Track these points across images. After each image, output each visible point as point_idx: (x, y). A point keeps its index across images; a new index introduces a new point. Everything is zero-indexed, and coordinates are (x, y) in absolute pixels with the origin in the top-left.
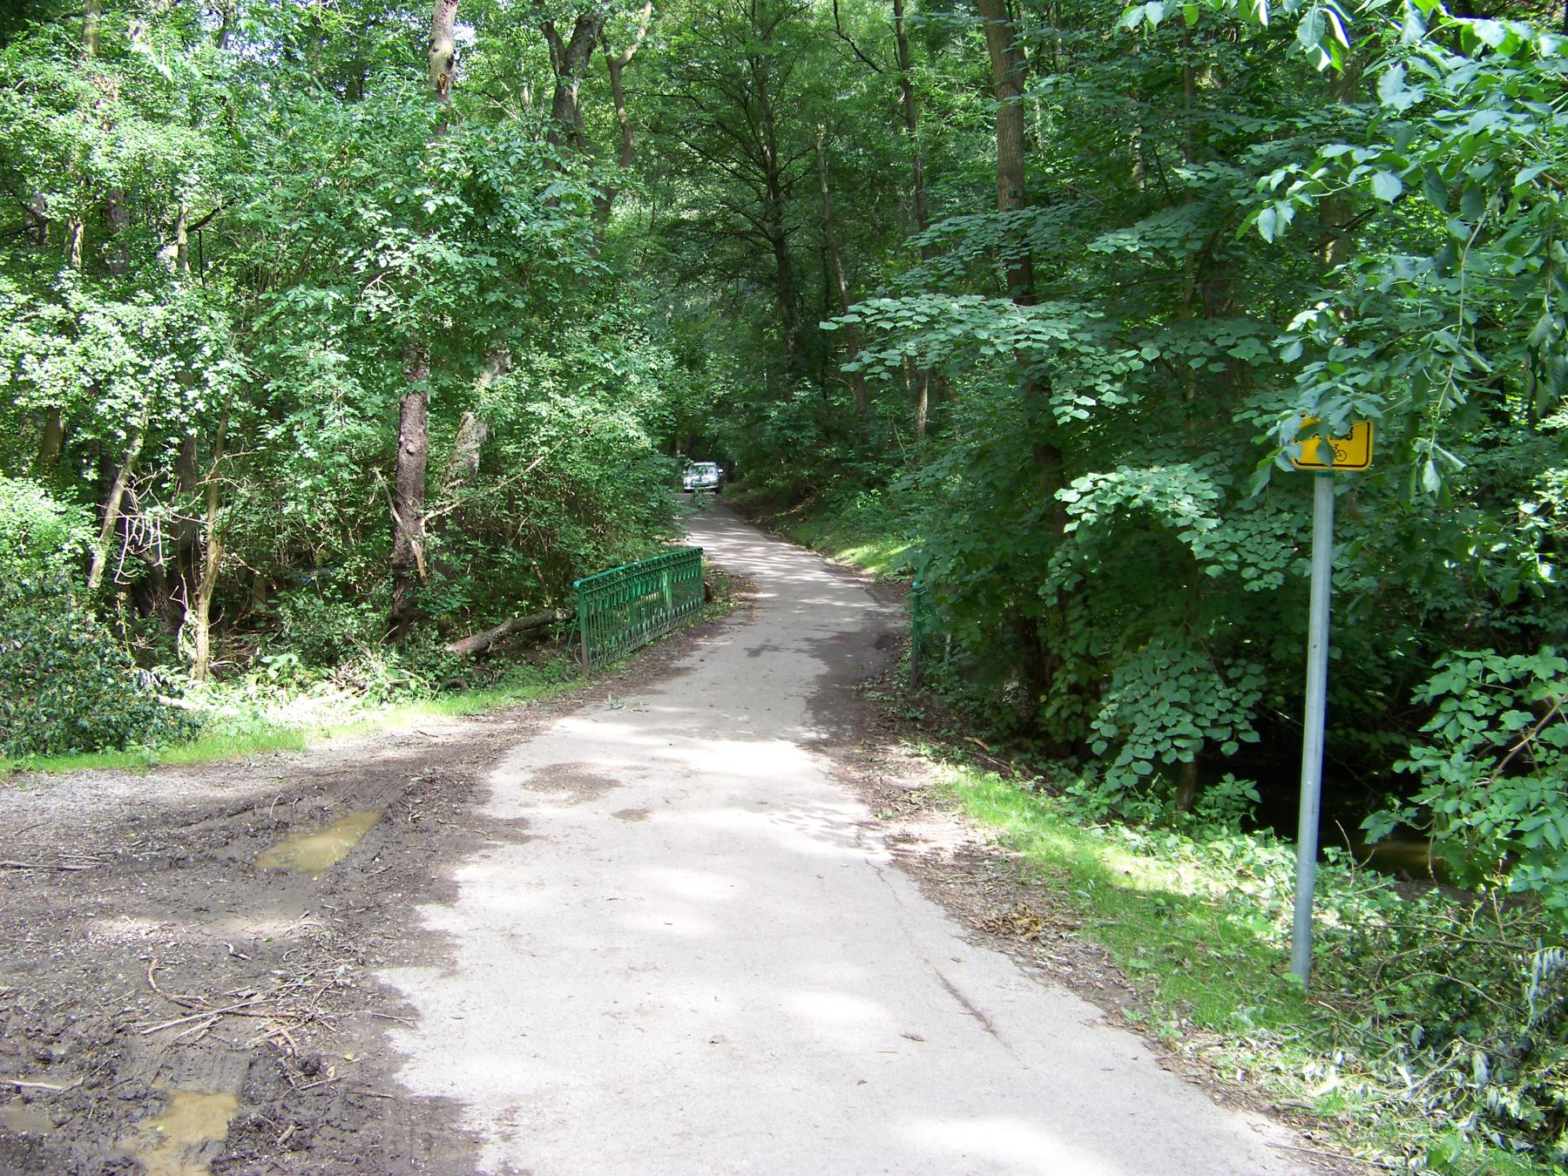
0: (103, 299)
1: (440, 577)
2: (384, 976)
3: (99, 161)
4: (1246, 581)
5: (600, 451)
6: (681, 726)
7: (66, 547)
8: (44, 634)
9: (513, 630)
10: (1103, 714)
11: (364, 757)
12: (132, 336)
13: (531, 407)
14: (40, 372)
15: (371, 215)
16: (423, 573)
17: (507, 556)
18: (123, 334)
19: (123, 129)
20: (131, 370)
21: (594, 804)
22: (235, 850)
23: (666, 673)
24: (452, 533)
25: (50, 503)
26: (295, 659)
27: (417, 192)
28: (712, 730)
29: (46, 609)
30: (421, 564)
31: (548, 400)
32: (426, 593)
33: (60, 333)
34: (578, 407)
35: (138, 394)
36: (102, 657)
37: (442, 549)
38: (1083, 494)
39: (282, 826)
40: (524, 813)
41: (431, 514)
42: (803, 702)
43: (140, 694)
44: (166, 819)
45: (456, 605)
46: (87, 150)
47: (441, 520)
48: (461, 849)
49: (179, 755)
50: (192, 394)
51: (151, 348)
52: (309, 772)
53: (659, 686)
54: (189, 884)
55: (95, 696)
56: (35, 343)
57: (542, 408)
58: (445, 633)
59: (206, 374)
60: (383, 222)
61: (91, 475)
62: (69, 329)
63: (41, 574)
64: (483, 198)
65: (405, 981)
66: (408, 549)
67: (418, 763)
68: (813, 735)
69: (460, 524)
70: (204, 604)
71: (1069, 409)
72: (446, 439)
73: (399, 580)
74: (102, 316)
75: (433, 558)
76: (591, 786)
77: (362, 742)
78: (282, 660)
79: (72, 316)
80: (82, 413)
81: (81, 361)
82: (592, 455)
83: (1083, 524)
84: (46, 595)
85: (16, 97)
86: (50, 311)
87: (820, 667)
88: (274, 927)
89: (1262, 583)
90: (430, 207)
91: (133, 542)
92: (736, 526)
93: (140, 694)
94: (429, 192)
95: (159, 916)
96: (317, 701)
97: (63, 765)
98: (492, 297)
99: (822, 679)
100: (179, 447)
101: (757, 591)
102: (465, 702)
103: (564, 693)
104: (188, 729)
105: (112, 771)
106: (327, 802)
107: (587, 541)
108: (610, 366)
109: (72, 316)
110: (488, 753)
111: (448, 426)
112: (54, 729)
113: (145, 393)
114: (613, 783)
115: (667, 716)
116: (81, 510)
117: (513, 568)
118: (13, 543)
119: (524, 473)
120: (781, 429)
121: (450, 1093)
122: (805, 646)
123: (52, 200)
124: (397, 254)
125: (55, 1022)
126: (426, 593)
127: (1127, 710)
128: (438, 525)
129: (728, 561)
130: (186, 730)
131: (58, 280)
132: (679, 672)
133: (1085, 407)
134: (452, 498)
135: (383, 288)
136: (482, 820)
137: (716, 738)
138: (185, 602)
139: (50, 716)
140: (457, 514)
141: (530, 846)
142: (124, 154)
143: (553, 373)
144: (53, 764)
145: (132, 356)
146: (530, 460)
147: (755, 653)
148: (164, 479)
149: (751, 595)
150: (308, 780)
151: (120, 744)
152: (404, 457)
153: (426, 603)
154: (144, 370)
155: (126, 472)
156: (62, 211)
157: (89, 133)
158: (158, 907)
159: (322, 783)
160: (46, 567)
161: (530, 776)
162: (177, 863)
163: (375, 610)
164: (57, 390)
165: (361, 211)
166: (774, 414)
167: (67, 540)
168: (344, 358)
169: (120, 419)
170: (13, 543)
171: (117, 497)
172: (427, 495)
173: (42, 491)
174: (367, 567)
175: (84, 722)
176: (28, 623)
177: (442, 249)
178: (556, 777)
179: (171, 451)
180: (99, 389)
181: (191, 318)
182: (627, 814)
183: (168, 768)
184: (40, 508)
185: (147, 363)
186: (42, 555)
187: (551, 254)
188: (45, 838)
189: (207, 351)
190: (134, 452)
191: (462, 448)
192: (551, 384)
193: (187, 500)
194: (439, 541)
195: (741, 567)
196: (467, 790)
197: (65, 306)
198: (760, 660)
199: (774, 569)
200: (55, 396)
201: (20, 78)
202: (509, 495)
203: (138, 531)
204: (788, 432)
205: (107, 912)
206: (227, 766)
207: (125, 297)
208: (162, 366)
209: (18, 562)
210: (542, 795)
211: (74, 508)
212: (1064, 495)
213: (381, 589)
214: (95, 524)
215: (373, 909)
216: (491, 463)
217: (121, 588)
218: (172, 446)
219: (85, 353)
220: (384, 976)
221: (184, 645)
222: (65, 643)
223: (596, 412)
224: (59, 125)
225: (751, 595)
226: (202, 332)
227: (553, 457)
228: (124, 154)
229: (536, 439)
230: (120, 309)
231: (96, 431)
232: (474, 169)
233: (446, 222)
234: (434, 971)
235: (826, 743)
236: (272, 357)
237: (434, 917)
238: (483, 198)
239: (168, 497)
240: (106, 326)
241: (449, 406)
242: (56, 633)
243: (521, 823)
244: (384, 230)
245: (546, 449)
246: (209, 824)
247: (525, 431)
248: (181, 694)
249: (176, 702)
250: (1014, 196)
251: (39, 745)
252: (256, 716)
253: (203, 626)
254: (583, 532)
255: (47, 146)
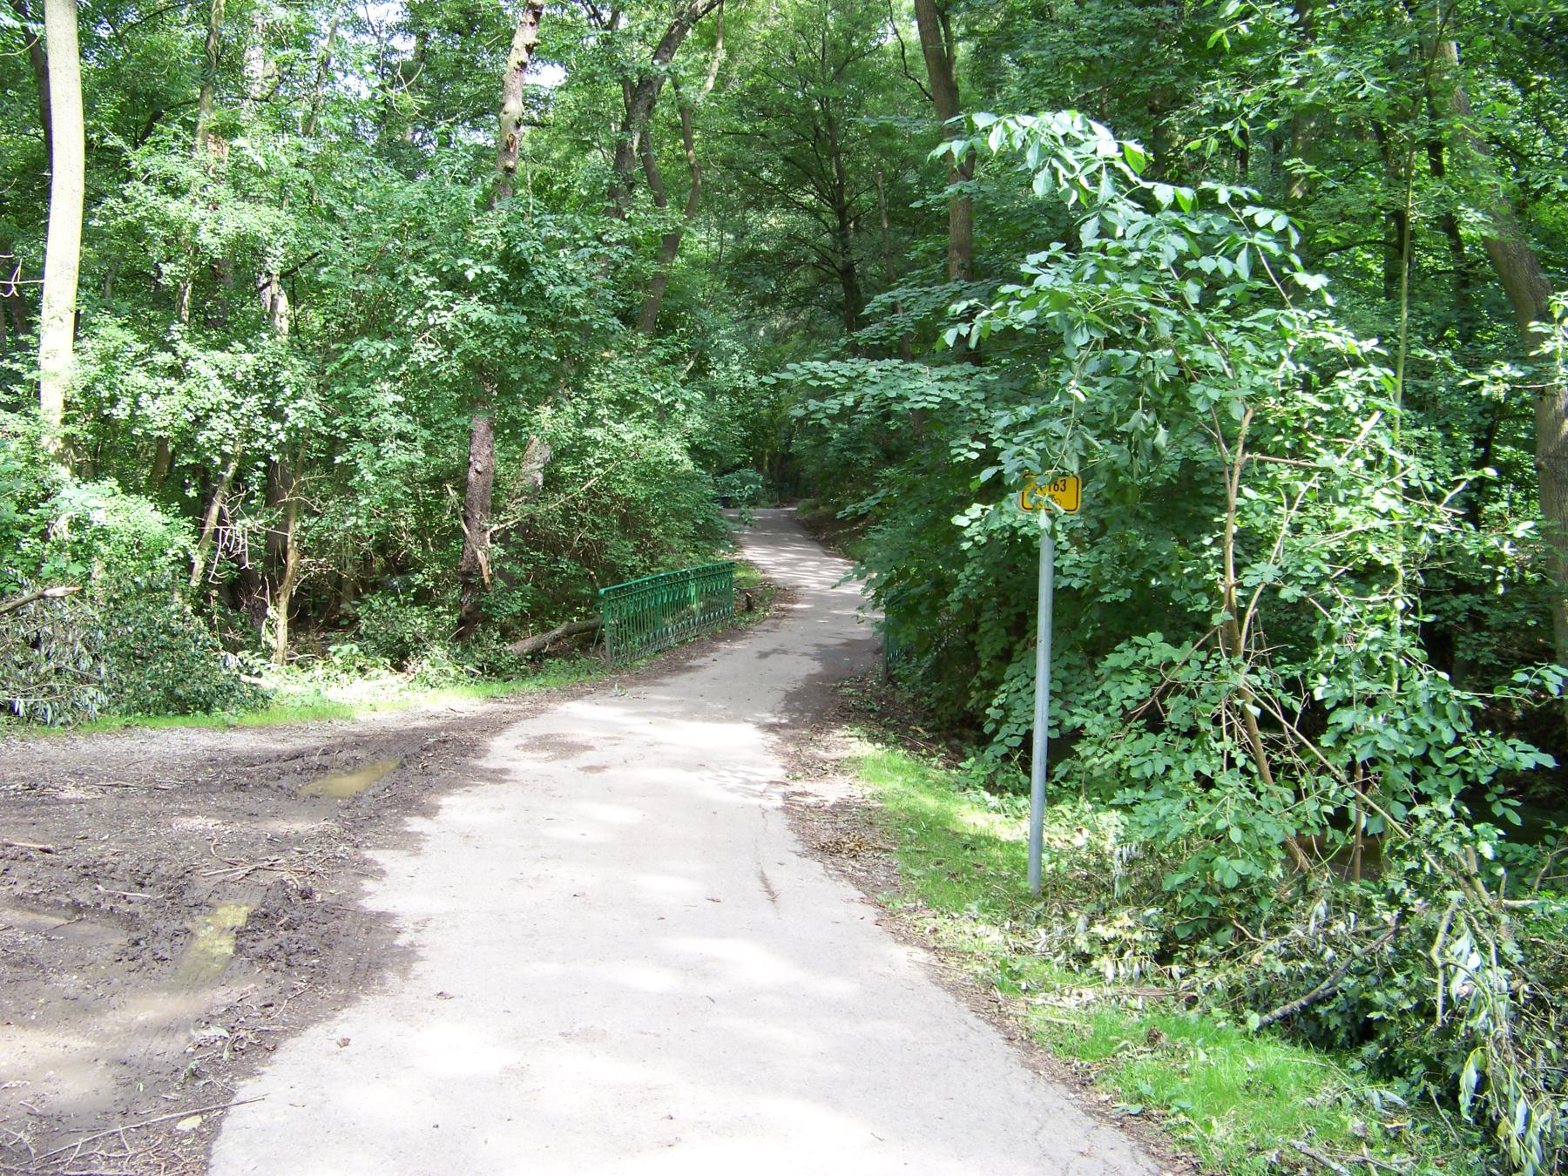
0: (205, 348)
1: (501, 583)
2: (368, 854)
3: (205, 237)
4: (1102, 594)
5: (649, 474)
6: (667, 709)
7: (171, 552)
8: (151, 622)
9: (568, 634)
10: (995, 702)
11: (401, 726)
12: (226, 378)
13: (588, 432)
14: (153, 408)
15: (422, 282)
16: (487, 580)
17: (564, 564)
18: (221, 377)
19: (224, 210)
20: (226, 407)
21: (566, 762)
22: (285, 782)
23: (678, 668)
24: (515, 544)
25: (158, 516)
26: (356, 649)
27: (460, 262)
28: (689, 715)
29: (152, 602)
30: (487, 571)
31: (603, 426)
32: (491, 597)
33: (170, 375)
34: (630, 432)
35: (231, 426)
36: (196, 642)
37: (505, 559)
38: (973, 521)
39: (322, 769)
40: (508, 765)
41: (496, 527)
42: (782, 694)
43: (225, 672)
44: (236, 761)
45: (516, 608)
46: (195, 229)
47: (507, 532)
48: (449, 786)
49: (252, 719)
50: (275, 426)
51: (242, 388)
52: (353, 734)
53: (666, 680)
54: (246, 801)
55: (189, 671)
56: (151, 384)
57: (596, 433)
58: (506, 634)
59: (287, 410)
60: (433, 286)
61: (192, 493)
62: (176, 372)
63: (149, 573)
64: (516, 266)
65: (382, 857)
66: (476, 559)
67: (437, 730)
68: (775, 720)
69: (525, 536)
70: (284, 602)
71: (964, 451)
72: (514, 460)
73: (467, 586)
74: (204, 363)
75: (497, 566)
76: (567, 749)
77: (400, 715)
78: (346, 648)
79: (180, 361)
80: (186, 440)
81: (185, 400)
82: (642, 478)
83: (976, 544)
84: (153, 590)
85: (142, 187)
86: (163, 358)
87: (816, 667)
88: (301, 826)
89: (1113, 597)
90: (470, 275)
91: (226, 548)
92: (799, 541)
93: (225, 672)
94: (469, 262)
95: (222, 817)
96: (375, 682)
97: (162, 722)
98: (522, 349)
99: (811, 678)
100: (265, 470)
101: (793, 602)
102: (497, 687)
103: (582, 684)
104: (260, 700)
105: (200, 729)
106: (359, 754)
107: (634, 553)
108: (657, 396)
109: (180, 361)
110: (495, 726)
111: (515, 447)
112: (155, 696)
113: (237, 425)
114: (591, 748)
115: (662, 703)
116: (182, 522)
117: (570, 577)
118: (128, 547)
119: (579, 491)
120: (842, 450)
121: (391, 910)
122: (813, 650)
123: (166, 269)
124: (443, 313)
125: (148, 866)
126: (491, 597)
127: (1012, 698)
128: (503, 538)
129: (780, 575)
130: (260, 701)
131: (168, 332)
132: (690, 669)
133: (976, 450)
134: (516, 512)
135: (431, 341)
136: (474, 769)
137: (692, 719)
138: (268, 600)
139: (154, 687)
140: (519, 528)
141: (504, 786)
142: (224, 231)
143: (609, 401)
144: (153, 723)
145: (227, 395)
146: (586, 479)
147: (764, 655)
148: (251, 496)
149: (790, 606)
150: (350, 739)
151: (207, 709)
152: (472, 475)
153: (489, 606)
154: (237, 407)
155: (223, 491)
156: (173, 278)
157: (197, 214)
158: (221, 811)
159: (360, 742)
160: (153, 568)
161: (523, 741)
162: (241, 787)
163: (450, 613)
164: (166, 423)
165: (413, 278)
166: (835, 436)
167: (171, 546)
168: (400, 399)
169: (216, 447)
170: (128, 547)
171: (215, 511)
172: (496, 509)
173: (152, 506)
174: (444, 574)
175: (180, 691)
176: (138, 612)
177: (480, 309)
178: (542, 743)
179: (258, 474)
180: (199, 422)
181: (276, 364)
182: (590, 769)
183: (243, 728)
184: (149, 520)
185: (239, 401)
186: (151, 558)
187: (574, 312)
188: (147, 769)
189: (288, 392)
190: (229, 474)
191: (527, 468)
192: (606, 412)
193: (271, 514)
194: (502, 552)
195: (791, 580)
196: (472, 748)
197: (175, 353)
198: (765, 661)
199: (821, 583)
200: (165, 428)
201: (145, 171)
202: (566, 511)
203: (230, 539)
204: (848, 454)
205: (184, 813)
206: (289, 729)
207: (222, 346)
208: (252, 403)
209: (132, 563)
210: (528, 754)
211: (175, 521)
212: (959, 520)
213: (453, 594)
214: (193, 533)
215: (374, 818)
216: (553, 481)
217: (214, 587)
218: (258, 469)
219: (189, 393)
220: (368, 854)
221: (267, 636)
222: (166, 629)
223: (646, 437)
224: (175, 208)
225: (790, 606)
226: (284, 376)
227: (606, 478)
228: (224, 231)
229: (591, 461)
230: (218, 356)
231: (196, 457)
232: (509, 242)
233: (485, 287)
234: (404, 853)
235: (782, 726)
236: (340, 396)
237: (415, 824)
238: (516, 266)
239: (252, 512)
240: (207, 371)
241: (511, 432)
242: (159, 621)
243: (505, 771)
244: (433, 292)
245: (600, 470)
246: (268, 765)
247: (583, 453)
248: (259, 675)
249: (254, 680)
250: (962, 267)
251: (145, 708)
252: (318, 692)
253: (282, 621)
254: (630, 545)
255: (165, 224)
